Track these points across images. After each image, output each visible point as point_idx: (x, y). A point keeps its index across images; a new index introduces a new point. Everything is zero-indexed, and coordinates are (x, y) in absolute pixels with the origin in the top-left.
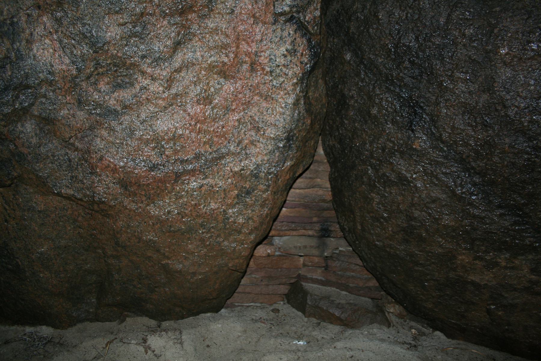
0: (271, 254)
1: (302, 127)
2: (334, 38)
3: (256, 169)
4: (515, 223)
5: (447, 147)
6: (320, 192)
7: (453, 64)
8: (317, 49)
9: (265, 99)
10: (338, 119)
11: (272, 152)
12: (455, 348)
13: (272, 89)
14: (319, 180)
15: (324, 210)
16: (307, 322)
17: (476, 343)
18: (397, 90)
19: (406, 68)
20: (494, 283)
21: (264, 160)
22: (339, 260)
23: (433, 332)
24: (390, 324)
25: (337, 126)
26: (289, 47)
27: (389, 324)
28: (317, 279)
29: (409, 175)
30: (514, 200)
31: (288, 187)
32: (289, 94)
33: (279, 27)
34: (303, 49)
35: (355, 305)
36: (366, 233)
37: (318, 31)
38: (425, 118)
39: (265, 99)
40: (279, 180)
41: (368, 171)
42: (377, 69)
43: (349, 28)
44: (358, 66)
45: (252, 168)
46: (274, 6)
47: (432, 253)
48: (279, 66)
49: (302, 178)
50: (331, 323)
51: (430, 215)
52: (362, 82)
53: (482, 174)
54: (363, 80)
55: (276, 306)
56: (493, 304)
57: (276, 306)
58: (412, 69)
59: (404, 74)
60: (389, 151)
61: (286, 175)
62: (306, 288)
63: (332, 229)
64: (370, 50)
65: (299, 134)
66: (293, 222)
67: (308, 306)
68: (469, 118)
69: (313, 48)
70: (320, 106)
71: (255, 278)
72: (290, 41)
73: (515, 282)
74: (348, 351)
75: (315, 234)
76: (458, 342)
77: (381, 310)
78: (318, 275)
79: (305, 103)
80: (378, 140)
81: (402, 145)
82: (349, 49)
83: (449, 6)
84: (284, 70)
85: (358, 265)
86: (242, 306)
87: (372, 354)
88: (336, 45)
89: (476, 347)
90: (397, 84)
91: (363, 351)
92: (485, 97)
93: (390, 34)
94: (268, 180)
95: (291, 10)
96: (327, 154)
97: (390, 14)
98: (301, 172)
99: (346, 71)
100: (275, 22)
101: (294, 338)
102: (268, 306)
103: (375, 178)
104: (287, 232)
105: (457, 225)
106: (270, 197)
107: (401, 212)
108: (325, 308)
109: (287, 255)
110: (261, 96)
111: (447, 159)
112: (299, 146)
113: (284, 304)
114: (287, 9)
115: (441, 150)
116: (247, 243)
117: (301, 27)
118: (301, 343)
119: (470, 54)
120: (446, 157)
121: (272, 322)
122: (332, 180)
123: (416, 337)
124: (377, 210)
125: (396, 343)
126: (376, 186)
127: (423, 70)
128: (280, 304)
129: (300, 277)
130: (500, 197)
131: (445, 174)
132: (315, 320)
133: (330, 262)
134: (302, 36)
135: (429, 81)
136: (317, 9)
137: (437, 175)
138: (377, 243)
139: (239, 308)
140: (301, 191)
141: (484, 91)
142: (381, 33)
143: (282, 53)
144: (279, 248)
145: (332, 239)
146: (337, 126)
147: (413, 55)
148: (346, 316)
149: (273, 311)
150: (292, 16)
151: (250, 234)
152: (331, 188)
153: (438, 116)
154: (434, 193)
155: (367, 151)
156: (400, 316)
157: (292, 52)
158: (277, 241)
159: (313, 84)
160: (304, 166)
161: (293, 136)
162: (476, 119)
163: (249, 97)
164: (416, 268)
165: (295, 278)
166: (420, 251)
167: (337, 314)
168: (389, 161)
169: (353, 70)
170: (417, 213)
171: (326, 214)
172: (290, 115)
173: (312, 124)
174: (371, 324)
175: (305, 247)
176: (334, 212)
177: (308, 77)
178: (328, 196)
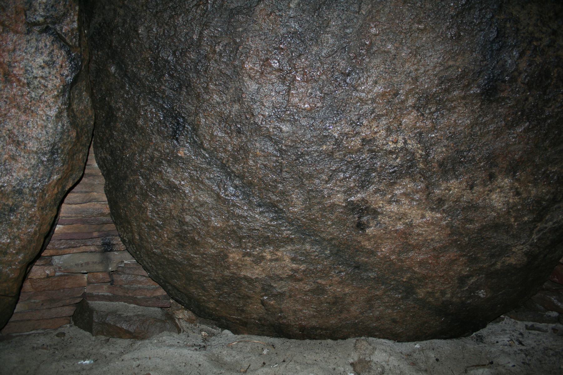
0: (50, 275)
1: (66, 139)
2: (98, 51)
3: (18, 184)
4: (272, 219)
5: (209, 154)
6: (98, 206)
7: (207, 77)
8: (78, 62)
9: (24, 112)
10: (107, 131)
11: (34, 167)
12: (239, 342)
13: (31, 101)
14: (95, 193)
15: (104, 223)
16: (94, 341)
17: (258, 335)
18: (161, 102)
19: (166, 81)
20: (264, 275)
21: (27, 175)
22: (124, 273)
23: (222, 331)
24: (180, 330)
25: (107, 138)
26: (47, 59)
27: (179, 330)
28: (103, 295)
29: (177, 183)
30: (270, 199)
31: (58, 202)
32: (50, 106)
33: (34, 37)
34: (63, 61)
35: (144, 316)
36: (144, 242)
37: (77, 43)
38: (187, 128)
39: (24, 112)
40: (45, 195)
41: (139, 181)
42: (140, 82)
43: (111, 41)
44: (122, 78)
45: (14, 184)
46: (26, 15)
47: (206, 254)
48: (36, 78)
49: (74, 192)
50: (121, 337)
51: (200, 218)
52: (128, 95)
53: (241, 177)
54: (128, 93)
55: (61, 330)
56: (265, 295)
57: (61, 330)
58: (172, 82)
59: (165, 86)
60: (157, 160)
61: (54, 190)
62: (92, 306)
63: (115, 242)
64: (133, 64)
65: (64, 147)
66: (71, 239)
67: (94, 324)
68: (225, 127)
69: (73, 60)
70: (86, 119)
71: (35, 302)
72: (47, 52)
73: (280, 272)
74: (135, 361)
75: (97, 249)
76: (243, 336)
77: (170, 318)
78: (104, 291)
79: (68, 116)
80: (146, 150)
81: (168, 154)
82: (113, 62)
83: (200, 24)
84: (43, 81)
85: (144, 276)
86: (22, 336)
87: (160, 360)
88: (101, 58)
89: (259, 338)
90: (159, 96)
91: (150, 358)
92: (236, 107)
93: (150, 48)
94: (33, 195)
95: (46, 21)
96: (100, 167)
97: (149, 29)
98: (71, 186)
99: (111, 84)
100: (29, 32)
101: (80, 359)
102: (52, 331)
103: (147, 187)
104: (66, 250)
105: (224, 226)
106: (37, 213)
107: (174, 218)
108: (112, 323)
109: (69, 274)
110: (19, 108)
111: (210, 165)
112: (65, 160)
113: (71, 326)
114: (41, 19)
115: (204, 157)
116: (15, 264)
117: (59, 38)
118: (87, 362)
119: (221, 68)
120: (209, 163)
121: (56, 347)
122: (108, 192)
123: (206, 339)
124: (151, 219)
125: (186, 346)
126: (148, 195)
127: (182, 82)
128: (66, 327)
129: (84, 295)
130: (258, 196)
131: (209, 179)
132: (103, 338)
133: (115, 277)
134: (61, 48)
135: (188, 93)
136: (74, 21)
137: (202, 181)
138: (154, 250)
139: (18, 338)
140: (78, 206)
141: (235, 101)
142: (141, 47)
143: (40, 64)
144: (60, 268)
145: (116, 253)
146: (107, 138)
147: (172, 69)
148: (135, 327)
149: (58, 335)
150: (47, 27)
151: (17, 253)
152: (108, 200)
153: (198, 125)
154: (201, 197)
155: (137, 161)
156: (190, 321)
157: (50, 64)
158: (57, 260)
159: (76, 96)
160: (74, 180)
161: (57, 149)
162: (230, 127)
163: (5, 110)
164: (194, 271)
165: (80, 297)
166: (196, 254)
167: (125, 326)
168: (158, 170)
169: (118, 82)
170: (188, 218)
171: (106, 228)
172: (52, 128)
173: (78, 137)
174: (161, 332)
175: (87, 263)
176: (113, 224)
177: (71, 89)
178: (107, 210)
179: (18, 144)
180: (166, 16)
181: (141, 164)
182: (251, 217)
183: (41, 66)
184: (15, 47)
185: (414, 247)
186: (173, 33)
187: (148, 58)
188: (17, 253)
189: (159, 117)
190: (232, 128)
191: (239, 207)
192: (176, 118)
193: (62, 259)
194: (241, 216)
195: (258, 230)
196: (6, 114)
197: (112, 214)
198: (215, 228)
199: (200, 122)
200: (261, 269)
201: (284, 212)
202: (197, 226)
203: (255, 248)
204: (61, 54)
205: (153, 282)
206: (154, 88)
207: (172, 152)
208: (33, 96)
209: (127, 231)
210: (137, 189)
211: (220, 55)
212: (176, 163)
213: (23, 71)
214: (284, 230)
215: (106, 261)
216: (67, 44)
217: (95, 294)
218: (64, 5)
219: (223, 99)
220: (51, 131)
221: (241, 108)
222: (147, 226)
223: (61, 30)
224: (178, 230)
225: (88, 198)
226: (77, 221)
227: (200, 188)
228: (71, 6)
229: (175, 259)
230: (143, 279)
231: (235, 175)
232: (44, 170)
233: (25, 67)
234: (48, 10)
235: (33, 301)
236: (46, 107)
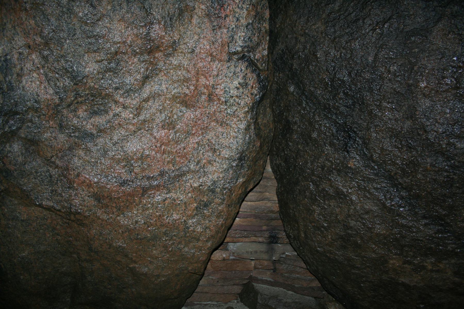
2: (279, 74)
3: (212, 185)
4: (438, 232)
5: (377, 165)
6: (269, 204)
8: (265, 83)
9: (220, 125)
11: (226, 170)
13: (227, 116)
14: (267, 194)
15: (272, 219)
19: (341, 99)
21: (220, 177)
22: (286, 264)
25: (283, 147)
26: (242, 81)
28: (266, 280)
30: (437, 212)
32: (241, 120)
35: (300, 304)
38: (358, 141)
39: (220, 125)
42: (317, 100)
43: (292, 65)
45: (209, 184)
46: (228, 46)
47: (366, 258)
48: (232, 97)
51: (364, 224)
52: (304, 110)
53: (408, 189)
54: (304, 109)
58: (346, 100)
60: (328, 169)
61: (239, 190)
62: (257, 288)
63: (280, 236)
65: (250, 155)
66: (245, 231)
68: (395, 141)
69: (262, 81)
71: (212, 279)
72: (242, 76)
78: (267, 276)
79: (255, 128)
80: (318, 160)
81: (339, 164)
82: (292, 82)
83: (376, 47)
84: (237, 100)
86: (201, 304)
92: (408, 123)
93: (327, 70)
94: (223, 194)
95: (243, 50)
97: (327, 54)
98: (251, 187)
99: (290, 101)
100: (229, 60)
104: (240, 239)
109: (240, 259)
110: (217, 122)
111: (378, 176)
112: (250, 165)
113: (238, 302)
114: (239, 49)
115: (373, 168)
116: (204, 250)
117: (252, 64)
120: (376, 175)
122: (279, 194)
124: (318, 220)
126: (317, 200)
128: (234, 302)
133: (278, 266)
135: (360, 110)
136: (265, 49)
139: (198, 306)
141: (407, 118)
144: (233, 253)
150: (244, 55)
151: (207, 241)
153: (369, 139)
154: (367, 205)
155: (309, 169)
158: (231, 246)
160: (254, 182)
161: (244, 157)
162: (401, 142)
164: (353, 271)
165: (246, 279)
166: (356, 256)
169: (296, 100)
170: (352, 223)
171: (274, 223)
172: (242, 139)
173: (261, 147)
175: (256, 252)
178: (276, 208)
179: (214, 151)
180: (343, 41)
181: (313, 171)
182: (415, 227)
183: (236, 87)
184: (218, 72)
185: (48, 82)
186: (349, 56)
187: (325, 79)
188: (207, 241)
189: (332, 130)
190: (403, 142)
191: (404, 218)
192: (347, 132)
193: (235, 246)
194: (403, 226)
195: (421, 240)
196: (207, 127)
197: (281, 212)
198: (378, 235)
199: (371, 136)
200: (419, 278)
201: (451, 226)
202: (360, 231)
203: (417, 257)
204: (253, 77)
205: (310, 274)
206: (329, 105)
207: (343, 163)
208: (229, 112)
209: (294, 228)
210: (307, 194)
211: (395, 75)
212: (346, 173)
213: (223, 91)
214: (450, 244)
215: (271, 251)
216: (258, 68)
217: (259, 278)
218: (258, 37)
219: (395, 115)
220: (241, 141)
221: (414, 125)
222: (314, 226)
223: (255, 57)
224: (342, 233)
225: (261, 197)
226: (250, 216)
227: (366, 196)
228: (263, 37)
229: (336, 259)
230: (300, 270)
231: (402, 187)
232: (233, 174)
233: (225, 88)
234: (246, 42)
235: (211, 277)
236: (238, 121)
